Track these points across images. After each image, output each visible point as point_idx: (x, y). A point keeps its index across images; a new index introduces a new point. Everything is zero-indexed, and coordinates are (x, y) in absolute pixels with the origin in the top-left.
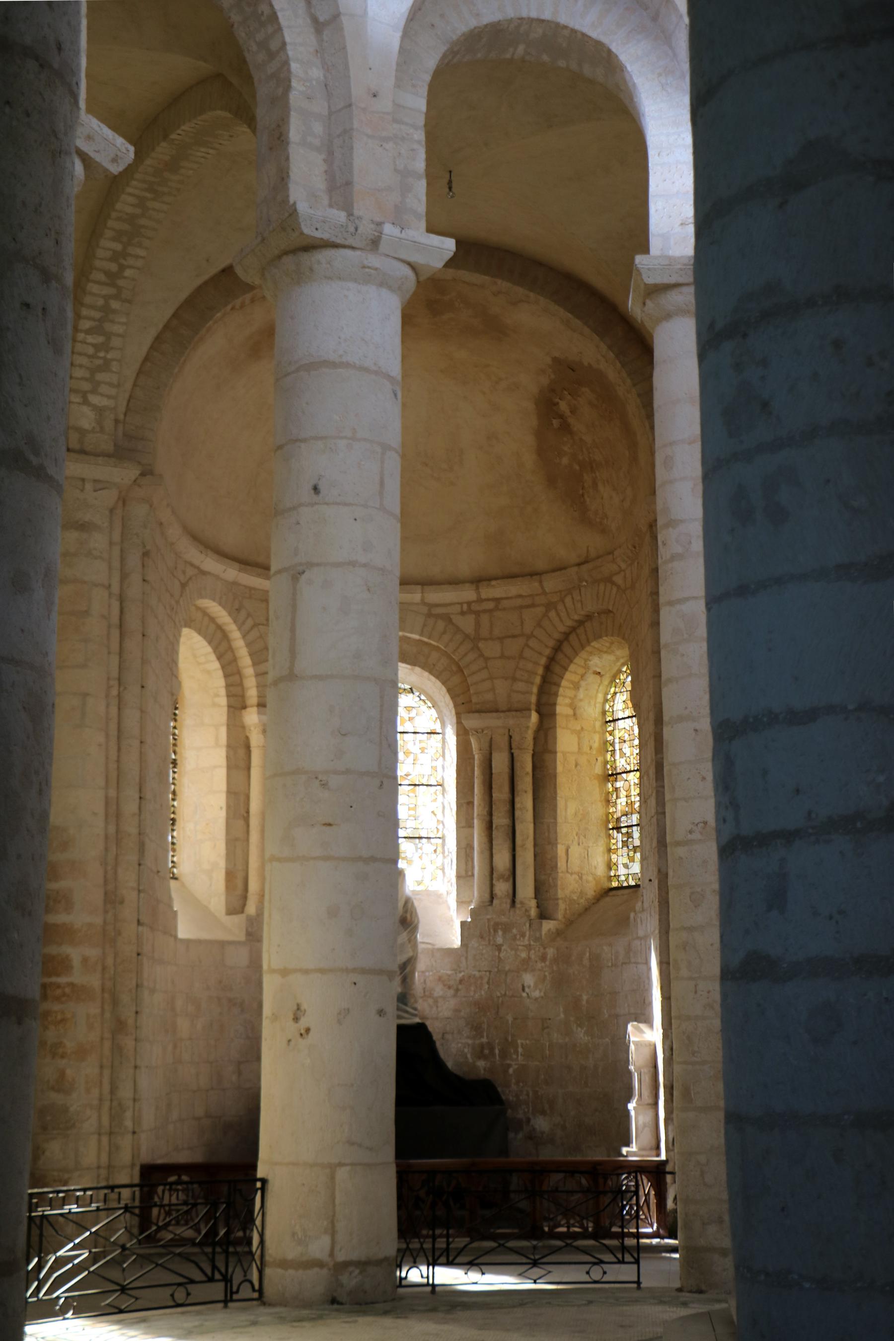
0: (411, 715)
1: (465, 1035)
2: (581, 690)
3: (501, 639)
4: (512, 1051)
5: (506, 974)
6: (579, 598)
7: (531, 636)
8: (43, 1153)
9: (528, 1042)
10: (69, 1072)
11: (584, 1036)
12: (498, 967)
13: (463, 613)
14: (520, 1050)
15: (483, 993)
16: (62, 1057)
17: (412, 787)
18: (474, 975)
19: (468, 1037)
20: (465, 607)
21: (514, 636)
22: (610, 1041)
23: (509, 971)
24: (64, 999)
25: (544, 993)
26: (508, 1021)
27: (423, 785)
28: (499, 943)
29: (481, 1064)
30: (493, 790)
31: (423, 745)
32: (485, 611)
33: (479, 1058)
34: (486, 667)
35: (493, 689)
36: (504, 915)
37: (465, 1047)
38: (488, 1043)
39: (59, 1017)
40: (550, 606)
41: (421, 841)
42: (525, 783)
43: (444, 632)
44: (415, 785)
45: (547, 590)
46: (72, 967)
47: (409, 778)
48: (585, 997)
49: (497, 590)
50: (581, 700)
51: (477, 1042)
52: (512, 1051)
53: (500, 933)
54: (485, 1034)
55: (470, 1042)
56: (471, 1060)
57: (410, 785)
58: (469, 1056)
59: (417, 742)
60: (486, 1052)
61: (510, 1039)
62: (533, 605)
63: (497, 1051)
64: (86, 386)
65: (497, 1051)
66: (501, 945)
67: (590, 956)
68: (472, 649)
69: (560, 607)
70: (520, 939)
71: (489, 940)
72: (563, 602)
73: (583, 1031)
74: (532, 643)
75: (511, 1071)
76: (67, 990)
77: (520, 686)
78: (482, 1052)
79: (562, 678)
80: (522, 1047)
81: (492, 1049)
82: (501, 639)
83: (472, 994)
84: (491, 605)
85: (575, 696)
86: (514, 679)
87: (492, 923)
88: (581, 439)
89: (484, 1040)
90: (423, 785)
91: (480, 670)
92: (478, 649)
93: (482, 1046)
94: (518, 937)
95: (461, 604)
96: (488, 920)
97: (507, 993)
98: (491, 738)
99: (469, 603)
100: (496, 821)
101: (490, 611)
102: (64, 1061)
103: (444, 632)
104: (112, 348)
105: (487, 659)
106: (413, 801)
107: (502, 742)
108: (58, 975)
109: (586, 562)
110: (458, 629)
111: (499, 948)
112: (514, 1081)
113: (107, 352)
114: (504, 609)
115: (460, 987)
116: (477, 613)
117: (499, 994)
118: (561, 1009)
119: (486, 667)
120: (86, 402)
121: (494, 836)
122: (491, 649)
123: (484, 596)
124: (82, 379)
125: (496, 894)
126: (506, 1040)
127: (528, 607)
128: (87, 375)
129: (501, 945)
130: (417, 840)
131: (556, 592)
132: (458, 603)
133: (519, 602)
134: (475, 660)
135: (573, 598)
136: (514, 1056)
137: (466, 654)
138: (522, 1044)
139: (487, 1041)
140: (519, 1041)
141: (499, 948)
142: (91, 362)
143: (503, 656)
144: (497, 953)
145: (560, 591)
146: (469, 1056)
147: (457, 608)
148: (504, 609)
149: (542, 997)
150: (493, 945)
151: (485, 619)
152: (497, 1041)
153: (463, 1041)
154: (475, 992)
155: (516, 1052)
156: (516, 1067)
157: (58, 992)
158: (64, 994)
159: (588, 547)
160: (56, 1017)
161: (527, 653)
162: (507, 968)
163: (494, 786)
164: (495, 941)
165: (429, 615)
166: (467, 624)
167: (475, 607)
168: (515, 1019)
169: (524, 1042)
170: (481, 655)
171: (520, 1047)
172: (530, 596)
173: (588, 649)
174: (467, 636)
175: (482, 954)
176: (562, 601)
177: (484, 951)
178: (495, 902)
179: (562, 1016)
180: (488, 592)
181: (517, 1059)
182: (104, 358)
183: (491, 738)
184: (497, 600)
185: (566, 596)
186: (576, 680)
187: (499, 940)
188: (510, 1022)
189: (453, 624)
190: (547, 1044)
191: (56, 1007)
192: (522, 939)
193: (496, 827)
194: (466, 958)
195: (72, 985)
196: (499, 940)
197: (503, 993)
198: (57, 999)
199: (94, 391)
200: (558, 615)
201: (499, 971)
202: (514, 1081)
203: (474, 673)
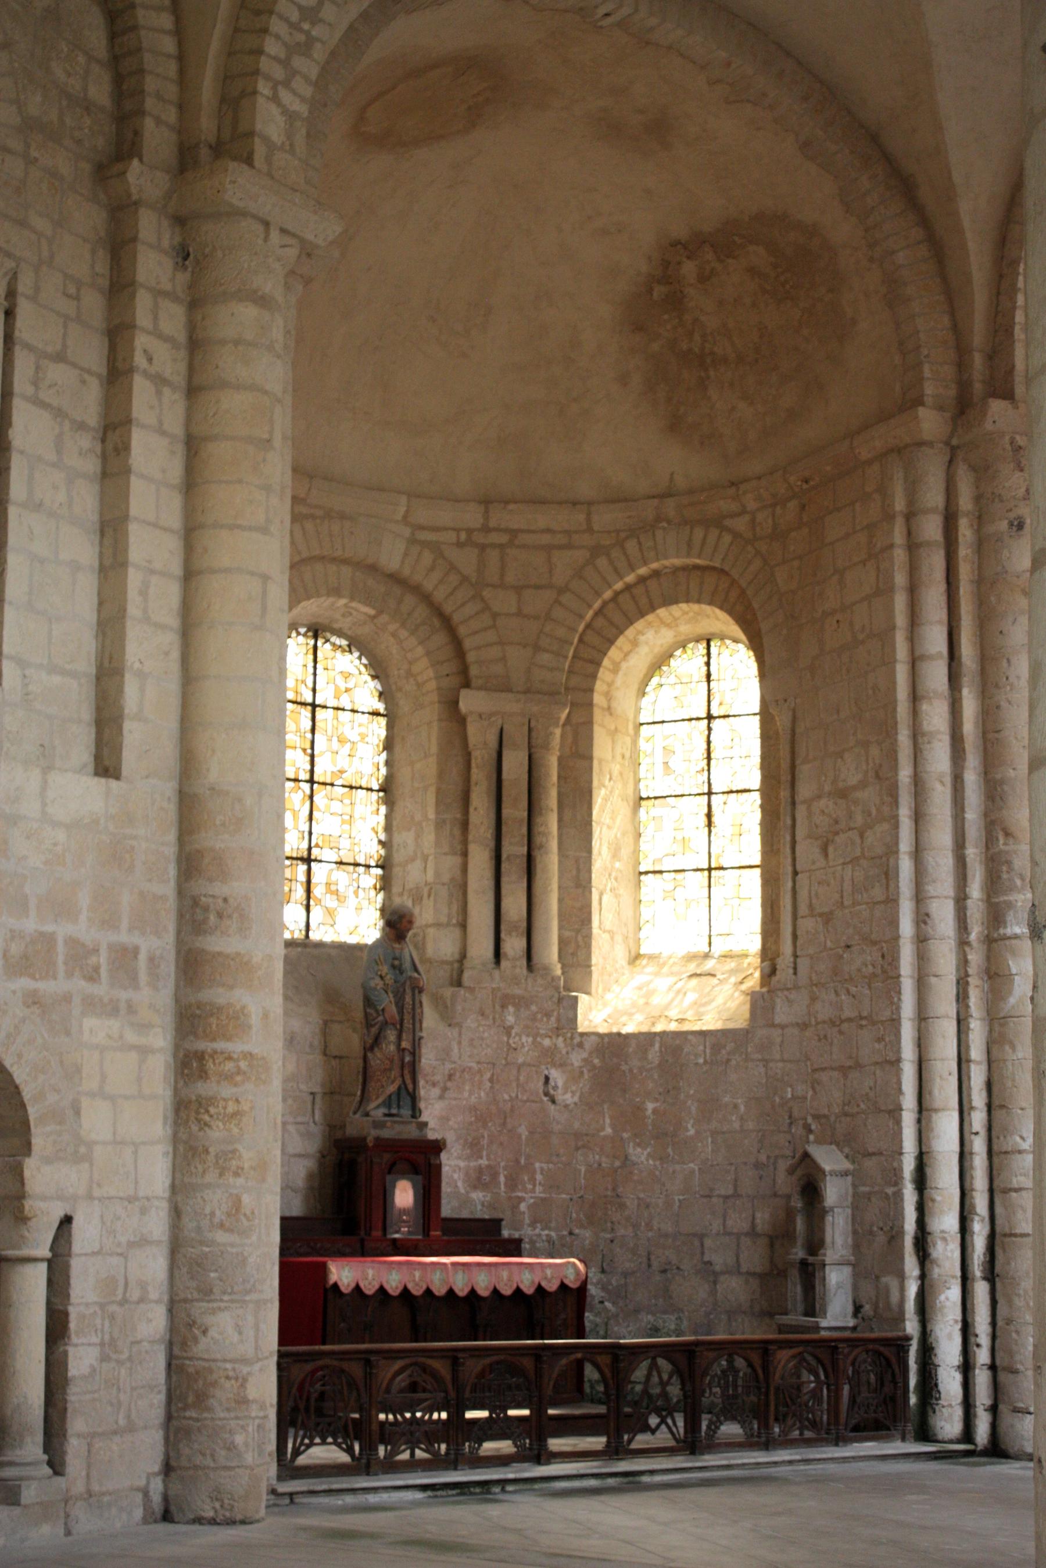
0: (350, 685)
1: (455, 1154)
2: (621, 673)
3: (518, 589)
4: (526, 1178)
5: (519, 1068)
6: (650, 544)
7: (561, 591)
8: (205, 1332)
9: (551, 1166)
10: (246, 1199)
11: (647, 1160)
12: (506, 1059)
13: (459, 545)
14: (539, 1177)
15: (482, 1094)
16: (236, 1174)
17: (347, 789)
18: (470, 1068)
19: (459, 1158)
20: (463, 536)
21: (538, 587)
22: (696, 1168)
23: (524, 1064)
24: (239, 1078)
25: (580, 1097)
26: (520, 1136)
27: (361, 788)
28: (508, 1024)
29: (477, 1196)
30: (504, 805)
31: (363, 730)
32: (493, 546)
33: (475, 1188)
34: (494, 626)
35: (504, 659)
36: (517, 984)
37: (454, 1171)
38: (489, 1167)
39: (231, 1108)
40: (596, 551)
41: (357, 869)
42: (551, 798)
43: (432, 569)
44: (351, 787)
45: (596, 528)
46: (250, 1027)
47: (344, 776)
48: (650, 1106)
49: (515, 518)
50: (617, 688)
51: (472, 1164)
52: (526, 1178)
53: (511, 1009)
54: (485, 1153)
55: (462, 1164)
56: (462, 1191)
57: (343, 786)
58: (460, 1184)
59: (356, 724)
60: (486, 1178)
61: (523, 1161)
62: (569, 546)
63: (502, 1179)
64: (279, 73)
65: (502, 1179)
66: (511, 1027)
67: (660, 1047)
68: (473, 597)
69: (615, 553)
70: (542, 1020)
71: (494, 1019)
72: (623, 548)
73: (645, 1153)
74: (566, 598)
75: (523, 1207)
76: (243, 1065)
77: (545, 658)
78: (479, 1179)
79: (605, 654)
80: (542, 1174)
81: (495, 1176)
82: (518, 589)
83: (466, 1094)
84: (504, 539)
85: (613, 682)
86: (537, 648)
87: (499, 994)
88: (696, 320)
89: (484, 1162)
90: (361, 788)
91: (485, 629)
92: (483, 600)
93: (480, 1170)
94: (539, 1016)
95: (458, 530)
96: (493, 989)
97: (520, 1096)
98: (502, 730)
99: (470, 531)
100: (507, 850)
101: (501, 546)
102: (240, 1181)
103: (432, 569)
104: (321, 20)
105: (495, 616)
106: (348, 810)
107: (516, 734)
108: (229, 1039)
109: (670, 495)
110: (452, 568)
111: (508, 1030)
112: (527, 1221)
113: (313, 24)
114: (524, 546)
115: (449, 1084)
116: (483, 548)
117: (506, 1097)
118: (608, 1121)
119: (494, 626)
120: (275, 99)
121: (503, 869)
122: (503, 601)
123: (492, 524)
124: (275, 58)
125: (505, 954)
126: (517, 1161)
127: (561, 547)
128: (282, 55)
129: (511, 1027)
130: (351, 868)
131: (609, 532)
132: (454, 529)
133: (546, 539)
134: (477, 614)
135: (640, 543)
136: (529, 1186)
137: (463, 605)
138: (542, 1169)
139: (486, 1163)
140: (537, 1165)
141: (508, 1030)
142: (291, 34)
143: (519, 614)
144: (505, 1039)
145: (618, 532)
146: (460, 1184)
147: (451, 537)
148: (524, 546)
149: (575, 1104)
150: (499, 1026)
151: (494, 555)
152: (502, 1164)
153: (453, 1163)
154: (471, 1093)
155: (533, 1180)
156: (532, 1201)
157: (229, 1066)
158: (239, 1072)
159: (672, 474)
160: (225, 1108)
161: (558, 613)
162: (520, 1060)
163: (504, 798)
164: (502, 1021)
165: (412, 541)
166: (467, 560)
167: (479, 538)
168: (531, 1133)
169: (545, 1166)
170: (487, 608)
171: (538, 1172)
172: (567, 533)
173: (650, 617)
174: (465, 579)
175: (482, 1039)
176: (621, 544)
177: (486, 1035)
178: (504, 963)
179: (609, 1131)
180: (500, 517)
181: (533, 1191)
182: (308, 33)
183: (502, 730)
184: (514, 533)
185: (627, 538)
186: (618, 660)
187: (510, 1019)
188: (524, 1137)
189: (444, 558)
190: (583, 1169)
191: (226, 1091)
192: (545, 1019)
193: (508, 857)
194: (460, 1043)
195: (249, 1056)
196: (510, 1019)
197: (514, 1095)
198: (229, 1078)
199: (287, 84)
200: (611, 562)
201: (507, 1064)
202: (527, 1221)
203: (475, 633)
